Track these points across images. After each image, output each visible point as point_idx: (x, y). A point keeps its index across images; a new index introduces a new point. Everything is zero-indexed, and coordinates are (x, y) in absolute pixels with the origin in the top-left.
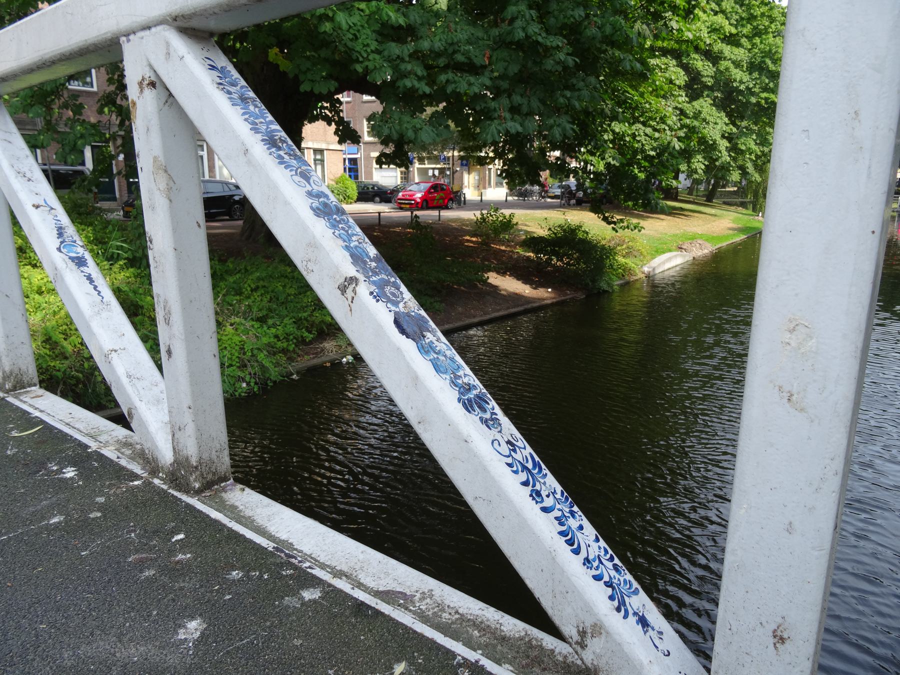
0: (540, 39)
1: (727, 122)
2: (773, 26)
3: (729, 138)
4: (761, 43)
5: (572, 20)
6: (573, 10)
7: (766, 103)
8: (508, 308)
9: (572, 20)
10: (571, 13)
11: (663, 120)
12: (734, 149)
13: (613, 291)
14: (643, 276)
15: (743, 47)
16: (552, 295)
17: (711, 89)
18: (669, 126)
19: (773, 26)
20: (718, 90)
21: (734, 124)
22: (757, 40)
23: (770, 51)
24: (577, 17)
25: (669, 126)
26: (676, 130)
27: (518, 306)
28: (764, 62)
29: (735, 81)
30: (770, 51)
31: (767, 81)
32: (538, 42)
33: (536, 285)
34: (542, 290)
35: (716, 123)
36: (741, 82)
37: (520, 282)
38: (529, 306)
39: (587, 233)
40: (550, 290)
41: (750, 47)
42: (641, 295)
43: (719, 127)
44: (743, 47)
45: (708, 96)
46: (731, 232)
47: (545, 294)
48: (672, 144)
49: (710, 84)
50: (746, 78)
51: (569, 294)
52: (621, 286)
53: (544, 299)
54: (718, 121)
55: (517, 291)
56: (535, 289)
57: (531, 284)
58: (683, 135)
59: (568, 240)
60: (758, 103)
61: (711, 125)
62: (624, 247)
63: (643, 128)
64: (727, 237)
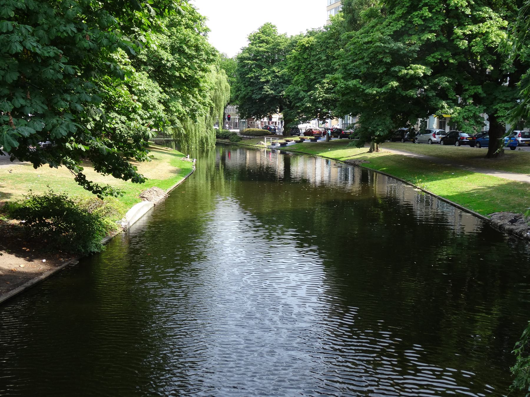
0: (38, 51)
1: (162, 91)
2: (183, 20)
3: (165, 103)
4: (177, 32)
5: (65, 34)
6: (65, 26)
7: (186, 76)
8: (8, 290)
9: (65, 34)
10: (64, 28)
11: (134, 110)
12: (167, 110)
13: (102, 251)
14: (120, 230)
15: (164, 34)
16: (48, 267)
17: (145, 64)
18: (139, 115)
19: (183, 20)
20: (150, 65)
21: (165, 91)
22: (174, 30)
23: (185, 39)
24: (70, 32)
25: (139, 115)
26: (146, 119)
27: (18, 285)
28: (181, 47)
29: (163, 59)
30: (185, 39)
31: (185, 61)
32: (36, 54)
33: (30, 257)
34: (36, 261)
35: (153, 92)
36: (168, 61)
37: (13, 256)
38: (28, 284)
39: (73, 203)
40: (44, 261)
41: (169, 34)
42: (121, 252)
43: (156, 94)
44: (164, 34)
45: (144, 70)
46: (172, 175)
47: (38, 267)
48: (147, 134)
49: (145, 60)
50: (171, 58)
51: (65, 262)
52: (106, 244)
53: (41, 274)
54: (155, 90)
55: (12, 268)
56: (29, 260)
57: (24, 257)
58: (152, 123)
59: (54, 207)
60: (180, 77)
61: (150, 93)
62: (103, 208)
63: (119, 116)
64: (171, 181)
